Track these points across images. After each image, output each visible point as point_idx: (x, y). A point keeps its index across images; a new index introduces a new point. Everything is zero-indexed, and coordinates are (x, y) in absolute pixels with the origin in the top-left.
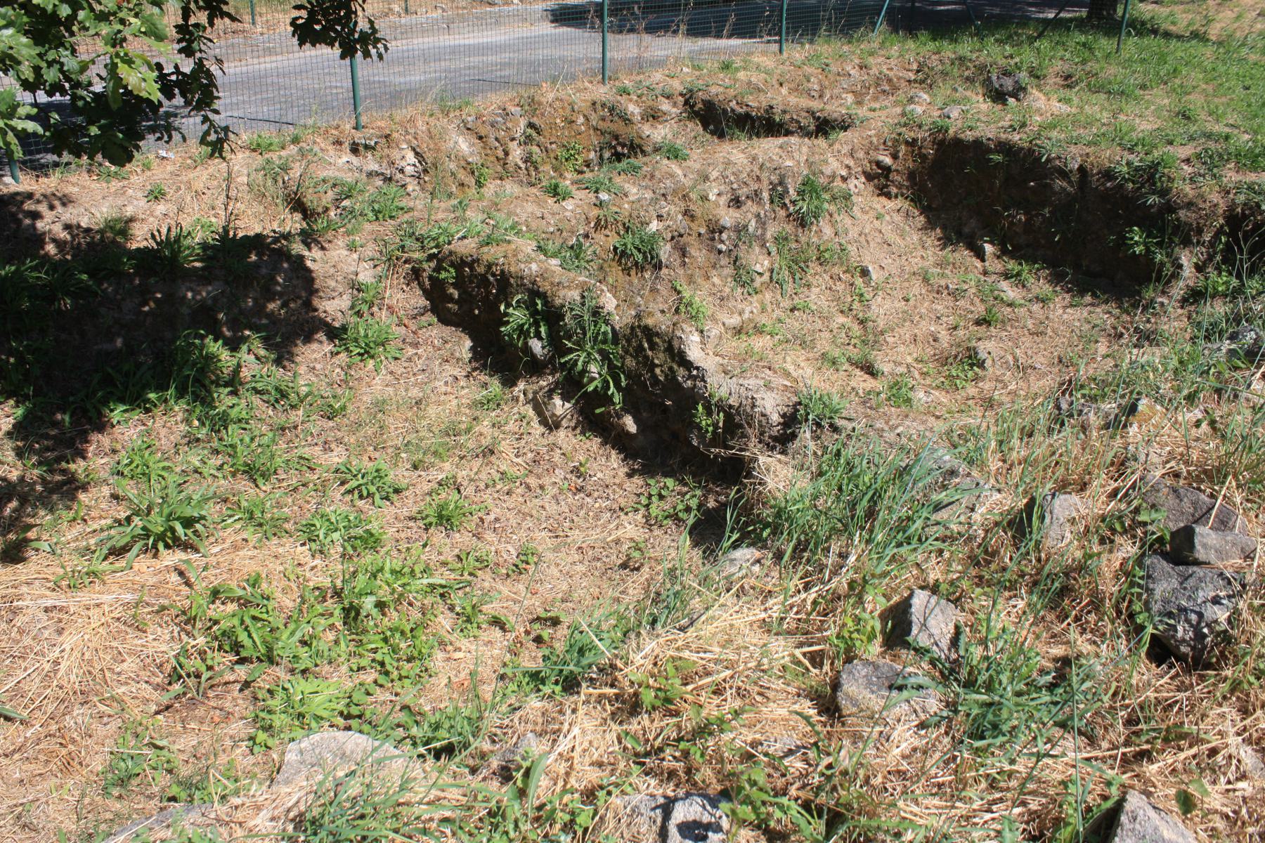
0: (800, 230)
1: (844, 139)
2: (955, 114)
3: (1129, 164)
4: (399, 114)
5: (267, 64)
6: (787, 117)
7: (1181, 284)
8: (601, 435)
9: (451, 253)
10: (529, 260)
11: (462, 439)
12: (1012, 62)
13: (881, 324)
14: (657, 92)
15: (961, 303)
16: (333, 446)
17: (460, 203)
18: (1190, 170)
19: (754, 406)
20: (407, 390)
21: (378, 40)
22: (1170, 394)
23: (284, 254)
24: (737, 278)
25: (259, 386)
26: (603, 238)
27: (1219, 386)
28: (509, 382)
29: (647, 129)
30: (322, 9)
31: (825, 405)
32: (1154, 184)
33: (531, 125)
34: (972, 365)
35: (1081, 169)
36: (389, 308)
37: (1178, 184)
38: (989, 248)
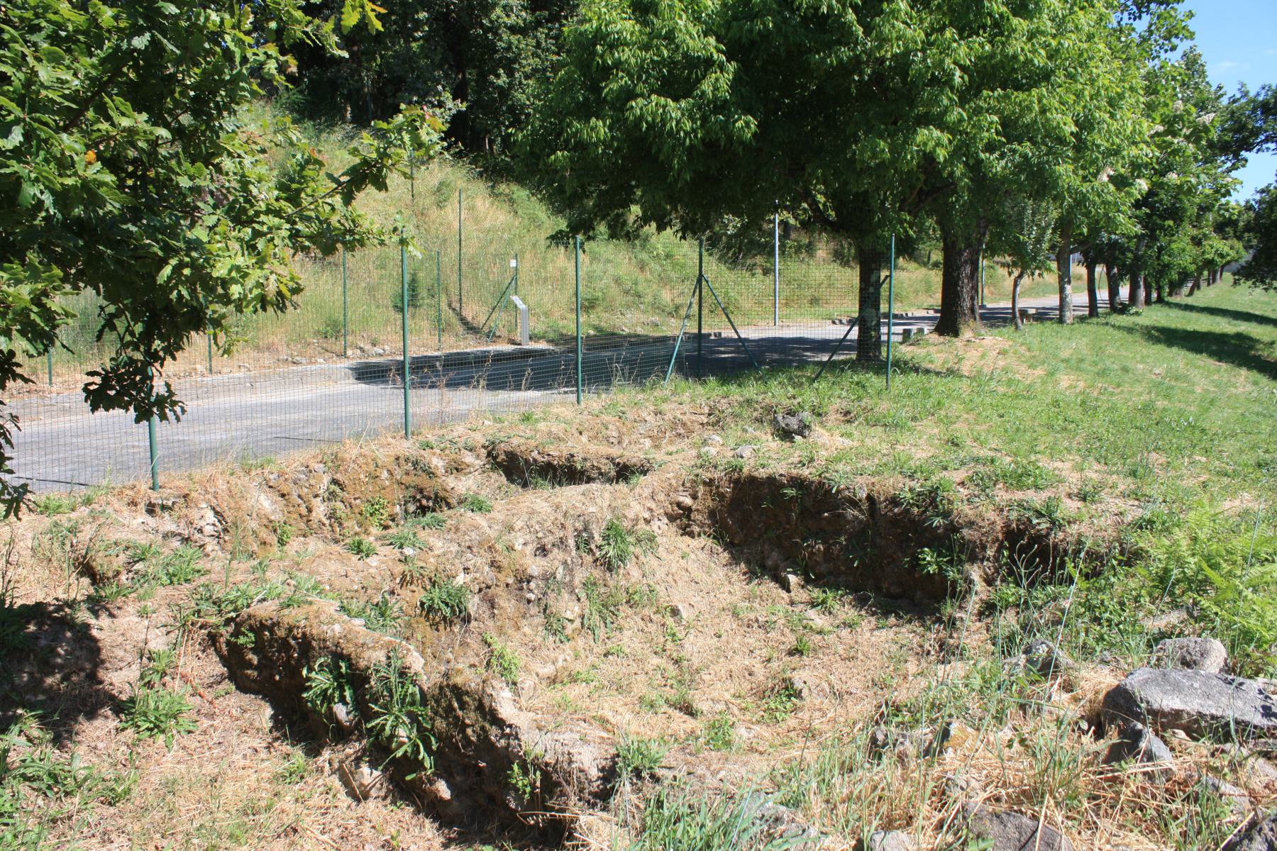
0: (608, 574)
1: (643, 483)
2: (747, 452)
3: (911, 490)
4: (198, 474)
5: (62, 423)
6: (588, 464)
7: (975, 598)
8: (414, 803)
9: (250, 616)
10: (332, 622)
11: (262, 818)
12: (795, 402)
13: (696, 662)
14: (460, 445)
15: (772, 635)
16: (113, 836)
17: (260, 563)
18: (966, 492)
19: (570, 762)
20: (201, 766)
21: (174, 403)
22: (979, 713)
23: (67, 623)
24: (548, 627)
25: (29, 772)
26: (410, 594)
27: (1022, 701)
28: (313, 752)
29: (451, 482)
30: (116, 375)
31: (644, 756)
32: (937, 507)
33: (335, 482)
34: (789, 696)
35: (870, 498)
36: (183, 677)
37: (957, 506)
38: (793, 579)
